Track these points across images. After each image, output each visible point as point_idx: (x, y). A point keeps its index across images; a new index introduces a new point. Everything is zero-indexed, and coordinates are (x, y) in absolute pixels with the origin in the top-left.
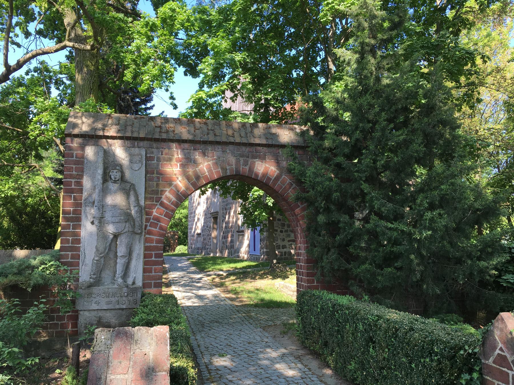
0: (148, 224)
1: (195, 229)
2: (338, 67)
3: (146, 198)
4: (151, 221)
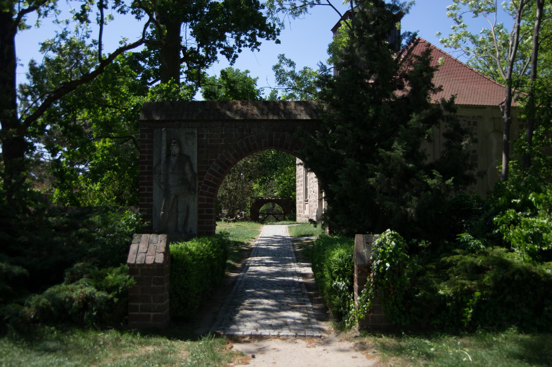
0: (201, 187)
1: (304, 275)
2: (71, 76)
3: (198, 167)
4: (203, 184)
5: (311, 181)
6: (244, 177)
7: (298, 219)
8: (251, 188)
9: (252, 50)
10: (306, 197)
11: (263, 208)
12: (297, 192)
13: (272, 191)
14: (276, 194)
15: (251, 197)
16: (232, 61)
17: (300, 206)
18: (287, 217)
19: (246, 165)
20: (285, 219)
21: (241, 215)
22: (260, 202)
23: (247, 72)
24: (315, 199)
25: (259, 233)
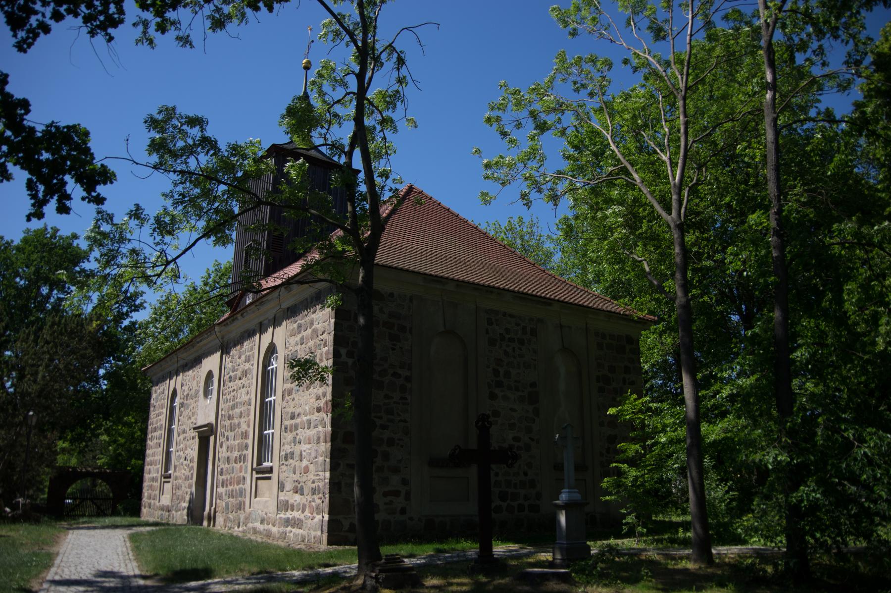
5: (182, 437)
6: (34, 420)
8: (51, 447)
9: (92, 33)
12: (148, 459)
13: (94, 457)
14: (99, 462)
16: (24, 41)
17: (151, 487)
18: (119, 507)
20: (115, 513)
21: (14, 507)
22: (65, 477)
24: (187, 473)
25: (48, 567)
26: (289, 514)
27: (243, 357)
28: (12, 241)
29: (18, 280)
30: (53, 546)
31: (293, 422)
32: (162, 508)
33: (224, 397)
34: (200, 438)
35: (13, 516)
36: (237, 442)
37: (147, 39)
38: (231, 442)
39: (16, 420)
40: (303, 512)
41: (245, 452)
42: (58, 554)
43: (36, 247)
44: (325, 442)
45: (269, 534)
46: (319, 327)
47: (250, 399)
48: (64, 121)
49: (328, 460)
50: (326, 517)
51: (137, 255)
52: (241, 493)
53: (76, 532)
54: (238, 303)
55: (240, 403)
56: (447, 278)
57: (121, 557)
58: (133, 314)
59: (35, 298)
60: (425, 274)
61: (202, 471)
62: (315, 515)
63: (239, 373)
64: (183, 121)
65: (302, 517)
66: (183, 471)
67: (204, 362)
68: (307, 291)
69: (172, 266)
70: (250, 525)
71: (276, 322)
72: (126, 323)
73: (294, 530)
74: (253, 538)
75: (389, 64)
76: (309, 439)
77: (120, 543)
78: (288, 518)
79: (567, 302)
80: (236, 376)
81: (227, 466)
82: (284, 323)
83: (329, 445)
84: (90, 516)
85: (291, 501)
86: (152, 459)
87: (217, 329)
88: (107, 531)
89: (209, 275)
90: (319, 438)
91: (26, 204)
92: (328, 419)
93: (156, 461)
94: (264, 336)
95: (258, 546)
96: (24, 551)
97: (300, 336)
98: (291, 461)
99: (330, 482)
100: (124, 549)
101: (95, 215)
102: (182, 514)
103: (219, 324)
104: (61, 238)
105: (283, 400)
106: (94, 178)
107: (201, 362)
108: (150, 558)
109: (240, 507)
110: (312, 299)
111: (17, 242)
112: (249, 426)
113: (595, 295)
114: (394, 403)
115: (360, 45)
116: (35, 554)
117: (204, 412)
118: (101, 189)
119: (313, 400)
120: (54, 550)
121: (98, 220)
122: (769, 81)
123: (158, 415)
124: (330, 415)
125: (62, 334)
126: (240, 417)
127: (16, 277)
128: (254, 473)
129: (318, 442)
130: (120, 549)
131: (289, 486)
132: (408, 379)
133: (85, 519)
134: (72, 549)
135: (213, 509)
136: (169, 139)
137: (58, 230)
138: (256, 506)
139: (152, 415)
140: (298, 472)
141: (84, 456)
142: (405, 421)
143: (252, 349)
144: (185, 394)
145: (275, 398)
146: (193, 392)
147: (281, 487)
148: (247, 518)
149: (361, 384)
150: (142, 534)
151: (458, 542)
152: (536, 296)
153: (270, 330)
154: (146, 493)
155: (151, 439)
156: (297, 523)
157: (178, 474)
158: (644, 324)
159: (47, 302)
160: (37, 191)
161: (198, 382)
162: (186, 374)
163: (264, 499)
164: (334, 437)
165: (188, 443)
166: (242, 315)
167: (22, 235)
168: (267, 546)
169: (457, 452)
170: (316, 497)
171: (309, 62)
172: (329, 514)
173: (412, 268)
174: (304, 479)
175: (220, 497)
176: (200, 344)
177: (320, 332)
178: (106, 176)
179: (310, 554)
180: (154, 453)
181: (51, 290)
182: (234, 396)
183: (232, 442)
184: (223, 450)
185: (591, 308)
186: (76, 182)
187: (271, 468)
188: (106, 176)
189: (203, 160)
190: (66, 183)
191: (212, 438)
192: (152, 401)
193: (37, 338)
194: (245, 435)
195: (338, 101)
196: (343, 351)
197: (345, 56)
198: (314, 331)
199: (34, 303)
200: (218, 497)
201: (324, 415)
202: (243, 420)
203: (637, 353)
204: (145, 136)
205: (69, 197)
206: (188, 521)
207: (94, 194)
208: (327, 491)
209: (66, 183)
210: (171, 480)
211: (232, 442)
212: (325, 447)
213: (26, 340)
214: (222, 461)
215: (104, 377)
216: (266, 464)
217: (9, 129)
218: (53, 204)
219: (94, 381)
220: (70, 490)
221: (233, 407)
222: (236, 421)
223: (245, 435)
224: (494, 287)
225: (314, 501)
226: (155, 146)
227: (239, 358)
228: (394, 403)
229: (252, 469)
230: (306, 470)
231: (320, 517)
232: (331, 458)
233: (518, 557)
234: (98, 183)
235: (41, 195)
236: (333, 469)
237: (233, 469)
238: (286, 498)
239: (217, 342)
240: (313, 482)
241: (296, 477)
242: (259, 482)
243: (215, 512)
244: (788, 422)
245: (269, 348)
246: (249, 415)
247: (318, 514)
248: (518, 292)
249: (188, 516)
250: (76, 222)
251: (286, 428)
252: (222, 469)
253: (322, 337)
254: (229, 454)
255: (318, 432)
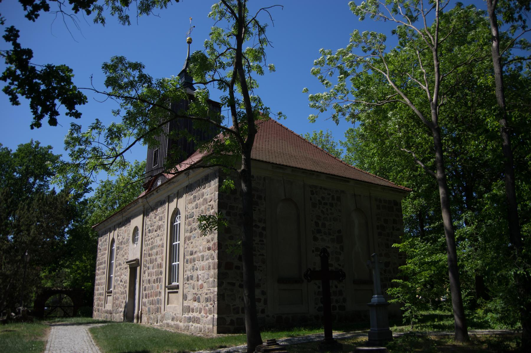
5: (118, 268)
6: (28, 259)
7: (96, 316)
8: (38, 275)
10: (109, 287)
11: (50, 300)
12: (97, 282)
14: (65, 285)
15: (37, 287)
17: (99, 299)
19: (457, 239)
20: (75, 315)
23: (50, 147)
24: (122, 290)
26: (191, 315)
27: (158, 218)
28: (11, 150)
29: (15, 174)
30: (43, 337)
31: (192, 257)
32: (106, 312)
33: (146, 243)
34: (130, 268)
35: (16, 318)
36: (154, 270)
37: (100, 19)
38: (151, 270)
39: (17, 258)
40: (200, 313)
41: (160, 276)
42: (47, 342)
43: (26, 154)
44: (214, 269)
45: (177, 327)
46: (208, 197)
47: (163, 244)
48: (56, 63)
49: (216, 280)
50: (216, 316)
51: (98, 152)
52: (159, 302)
53: (56, 327)
54: (152, 186)
55: (157, 246)
56: (286, 166)
57: (87, 343)
58: (85, 194)
59: (26, 185)
60: (273, 163)
61: (132, 288)
62: (208, 314)
63: (155, 227)
64: (127, 66)
65: (199, 316)
66: (120, 289)
67: (132, 221)
68: (202, 172)
69: (119, 158)
70: (165, 322)
71: (179, 195)
72: (82, 200)
73: (194, 324)
74: (168, 330)
75: (254, 30)
76: (203, 267)
77: (85, 334)
78: (190, 317)
79: (358, 180)
80: (153, 229)
81: (148, 285)
82: (185, 196)
83: (216, 271)
84: (62, 317)
85: (192, 307)
86: (99, 281)
87: (140, 201)
88: (75, 326)
89: (132, 169)
90: (209, 267)
91: (30, 118)
92: (215, 254)
93: (102, 283)
94: (171, 204)
95: (173, 335)
96: (26, 340)
97: (195, 203)
98: (191, 281)
99: (218, 294)
100: (88, 338)
101: (71, 127)
102: (120, 316)
103: (142, 197)
104: (41, 148)
105: (185, 243)
106: (74, 99)
107: (130, 222)
108: (106, 344)
109: (158, 310)
110: (202, 180)
111: (14, 150)
112: (162, 260)
113: (371, 177)
114: (256, 244)
115: (238, 16)
116: (33, 342)
117: (133, 252)
118: (78, 108)
119: (205, 243)
120: (44, 339)
121: (72, 130)
122: (494, 35)
123: (103, 255)
124: (217, 251)
125: (44, 205)
126: (157, 254)
127: (14, 172)
128: (167, 289)
129: (209, 268)
130: (85, 338)
131: (190, 297)
132: (264, 229)
133: (57, 320)
134: (56, 338)
135: (140, 312)
136: (119, 75)
137: (40, 143)
138: (168, 310)
139: (99, 254)
140: (196, 288)
141: (55, 281)
142: (263, 255)
143: (163, 212)
144: (120, 241)
145: (180, 242)
146: (125, 240)
147: (185, 297)
148: (162, 317)
149: (239, 230)
150: (96, 328)
151: (300, 330)
152: (340, 176)
153: (175, 200)
154: (96, 303)
155: (99, 270)
156: (196, 320)
157: (116, 290)
158: (404, 193)
159: (33, 188)
160: (37, 109)
161: (128, 234)
162: (120, 229)
163: (174, 305)
164: (220, 266)
165: (123, 272)
166: (157, 192)
167: (17, 148)
168: (179, 335)
169: (309, 273)
170: (208, 303)
171: (190, 39)
172: (218, 314)
173: (264, 160)
174: (200, 292)
175: (144, 304)
176: (130, 210)
177: (208, 201)
178: (81, 99)
179: (208, 340)
180: (101, 278)
181: (35, 180)
182: (152, 242)
183: (152, 270)
184: (145, 275)
185: (373, 183)
186: (62, 103)
187: (178, 286)
188: (81, 99)
189: (143, 90)
190: (55, 105)
191: (138, 268)
192: (99, 246)
193: (29, 207)
194: (160, 266)
195: (222, 54)
196: (224, 212)
197: (228, 25)
198: (207, 197)
199: (25, 188)
200: (143, 304)
201: (213, 252)
202: (158, 256)
203: (400, 210)
204: (102, 77)
205: (57, 114)
206: (124, 319)
207: (74, 111)
208: (216, 300)
209: (55, 105)
210: (112, 294)
211: (152, 270)
212: (214, 272)
213: (22, 209)
214: (145, 282)
215: (68, 232)
216: (174, 284)
217: (18, 68)
218: (46, 119)
219: (61, 235)
220: (48, 302)
221: (151, 249)
222: (154, 257)
223: (160, 266)
224: (314, 171)
225: (207, 306)
226: (111, 82)
227: (155, 218)
228: (256, 244)
229: (165, 287)
230: (202, 287)
231: (212, 316)
232: (218, 279)
233: (344, 339)
234: (76, 103)
235: (39, 111)
236: (220, 285)
237: (152, 287)
238: (189, 305)
239: (142, 208)
240: (206, 294)
241: (195, 291)
242: (170, 295)
243: (141, 314)
244: (523, 249)
245: (174, 211)
246: (162, 253)
247: (210, 314)
248: (329, 174)
249: (124, 317)
250: (53, 138)
251: (187, 261)
252: (145, 287)
253: (209, 203)
254: (149, 278)
255: (209, 263)
